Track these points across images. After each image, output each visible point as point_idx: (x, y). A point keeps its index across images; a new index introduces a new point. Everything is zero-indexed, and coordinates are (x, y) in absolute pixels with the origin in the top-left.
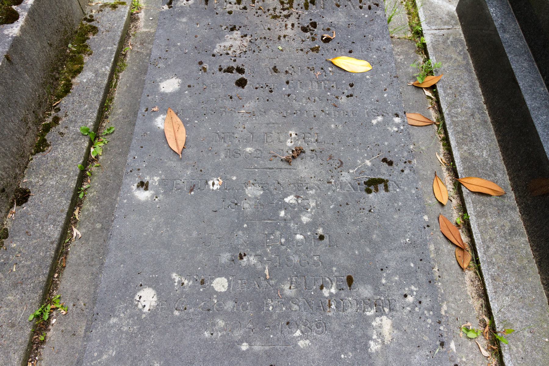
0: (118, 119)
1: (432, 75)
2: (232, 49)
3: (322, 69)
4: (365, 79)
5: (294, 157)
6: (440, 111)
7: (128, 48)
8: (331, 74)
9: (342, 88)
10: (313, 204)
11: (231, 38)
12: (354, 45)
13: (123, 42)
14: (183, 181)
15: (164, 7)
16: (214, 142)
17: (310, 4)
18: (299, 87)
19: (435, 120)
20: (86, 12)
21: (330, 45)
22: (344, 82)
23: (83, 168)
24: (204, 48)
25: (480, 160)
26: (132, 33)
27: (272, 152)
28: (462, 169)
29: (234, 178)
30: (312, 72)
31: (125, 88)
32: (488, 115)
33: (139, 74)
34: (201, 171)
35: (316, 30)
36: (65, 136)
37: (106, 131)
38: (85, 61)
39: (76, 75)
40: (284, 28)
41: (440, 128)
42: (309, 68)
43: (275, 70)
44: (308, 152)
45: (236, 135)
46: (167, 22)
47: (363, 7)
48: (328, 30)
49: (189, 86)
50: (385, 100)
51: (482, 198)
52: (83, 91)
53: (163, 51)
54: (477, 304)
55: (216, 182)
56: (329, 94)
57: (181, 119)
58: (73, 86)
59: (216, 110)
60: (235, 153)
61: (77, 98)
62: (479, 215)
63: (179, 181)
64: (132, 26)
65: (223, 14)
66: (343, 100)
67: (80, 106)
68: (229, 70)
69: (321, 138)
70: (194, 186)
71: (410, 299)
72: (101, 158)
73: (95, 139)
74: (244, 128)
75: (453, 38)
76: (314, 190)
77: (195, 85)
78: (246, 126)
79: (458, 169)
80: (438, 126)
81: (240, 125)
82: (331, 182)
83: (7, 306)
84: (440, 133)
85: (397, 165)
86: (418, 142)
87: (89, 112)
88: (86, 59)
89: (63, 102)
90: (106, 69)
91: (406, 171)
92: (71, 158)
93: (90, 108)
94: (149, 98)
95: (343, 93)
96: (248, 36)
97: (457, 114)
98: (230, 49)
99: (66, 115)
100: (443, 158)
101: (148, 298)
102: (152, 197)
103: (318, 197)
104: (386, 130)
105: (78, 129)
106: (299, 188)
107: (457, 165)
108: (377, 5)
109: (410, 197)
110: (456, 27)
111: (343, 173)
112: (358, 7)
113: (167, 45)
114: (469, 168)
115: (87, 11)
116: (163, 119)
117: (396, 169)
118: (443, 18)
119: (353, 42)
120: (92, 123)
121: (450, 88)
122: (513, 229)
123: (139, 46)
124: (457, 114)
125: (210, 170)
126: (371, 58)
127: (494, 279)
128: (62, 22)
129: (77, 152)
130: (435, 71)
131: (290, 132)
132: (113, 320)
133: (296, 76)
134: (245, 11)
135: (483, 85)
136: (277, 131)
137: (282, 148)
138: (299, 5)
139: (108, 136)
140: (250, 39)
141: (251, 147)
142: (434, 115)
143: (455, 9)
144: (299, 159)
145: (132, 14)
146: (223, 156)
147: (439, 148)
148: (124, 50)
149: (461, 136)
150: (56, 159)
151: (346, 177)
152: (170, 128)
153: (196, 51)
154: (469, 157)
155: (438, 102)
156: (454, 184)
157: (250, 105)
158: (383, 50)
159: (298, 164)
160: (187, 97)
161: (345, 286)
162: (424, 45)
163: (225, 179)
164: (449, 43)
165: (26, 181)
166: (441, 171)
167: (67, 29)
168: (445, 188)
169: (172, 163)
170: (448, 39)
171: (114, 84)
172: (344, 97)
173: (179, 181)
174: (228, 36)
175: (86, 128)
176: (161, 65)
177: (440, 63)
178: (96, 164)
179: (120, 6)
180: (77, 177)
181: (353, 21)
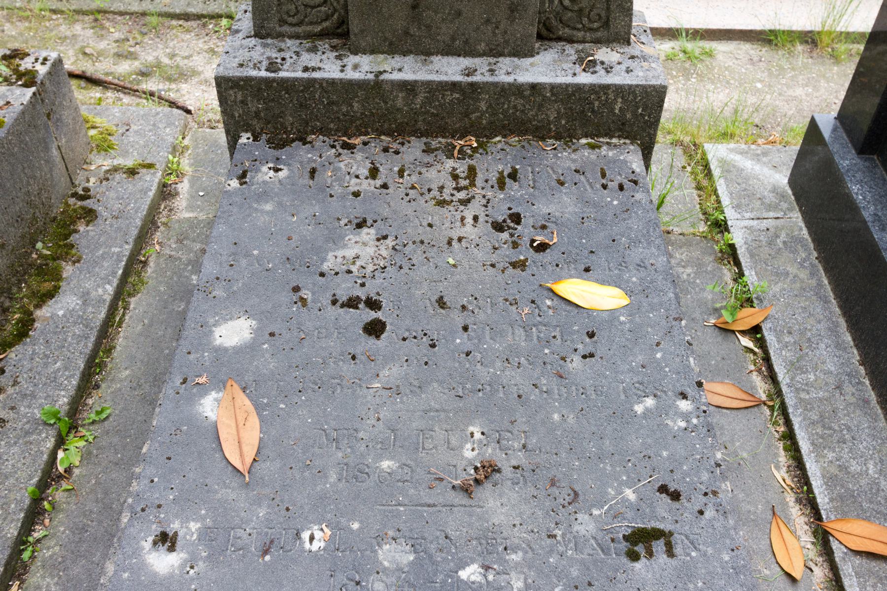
0: (120, 390)
1: (752, 306)
2: (358, 263)
3: (533, 302)
4: (617, 323)
5: (477, 482)
6: (772, 377)
7: (152, 250)
8: (551, 312)
9: (572, 341)
11: (356, 242)
12: (593, 257)
13: (149, 225)
14: (249, 535)
15: (231, 182)
16: (316, 449)
17: (507, 180)
18: (488, 338)
19: (764, 397)
20: (77, 183)
21: (546, 257)
22: (576, 328)
23: (38, 493)
24: (304, 260)
25: (863, 482)
26: (163, 220)
27: (433, 470)
28: (827, 500)
29: (356, 526)
30: (514, 308)
31: (140, 327)
32: (870, 387)
33: (170, 300)
34: (288, 509)
35: (519, 227)
36: (8, 425)
37: (93, 416)
38: (64, 276)
39: (44, 302)
40: (458, 224)
41: (775, 414)
42: (506, 300)
43: (441, 303)
44: (507, 471)
45: (361, 435)
46: (235, 210)
47: (609, 186)
48: (544, 227)
49: (272, 334)
50: (659, 364)
51: (874, 565)
52: (55, 333)
53: (225, 265)
55: (318, 535)
56: (547, 351)
57: (251, 400)
58: (36, 325)
59: (323, 383)
60: (357, 472)
61: (40, 348)
63: (240, 532)
64: (162, 207)
65: (343, 197)
66: (576, 363)
67: (46, 365)
68: (352, 303)
70: (272, 542)
72: (76, 471)
73: (69, 432)
74: (379, 419)
75: (788, 234)
76: (520, 554)
77: (284, 332)
78: (381, 416)
79: (819, 500)
80: (772, 408)
81: (372, 412)
82: (555, 536)
84: (775, 423)
85: (689, 500)
86: (732, 441)
87: (62, 376)
88: (68, 270)
89: (13, 355)
90: (105, 291)
91: (709, 514)
92: (16, 472)
93: (66, 368)
94: (191, 357)
95: (576, 350)
96: (390, 239)
97: (807, 384)
98: (354, 263)
99: (15, 383)
100: (786, 476)
102: (182, 566)
103: (530, 568)
104: (663, 426)
105: (36, 411)
107: (816, 491)
108: (635, 182)
109: (720, 570)
110: (791, 215)
111: (580, 516)
112: (598, 186)
113: (234, 254)
114: (841, 498)
115: (80, 179)
116: (216, 400)
117: (689, 507)
118: (764, 197)
119: (592, 252)
120: (66, 400)
121: (790, 333)
123: (174, 246)
124: (807, 384)
125: (307, 508)
126: (628, 281)
128: (30, 203)
129: (28, 461)
130: (757, 298)
131: (471, 429)
133: (481, 316)
134: (385, 191)
135: (854, 326)
136: (445, 426)
137: (454, 463)
138: (487, 181)
139: (96, 427)
140: (394, 243)
141: (392, 458)
142: (761, 388)
143: (786, 181)
144: (488, 485)
145: (165, 185)
146: (333, 478)
147: (776, 455)
148: (143, 252)
149: (819, 430)
151: (586, 525)
152: (230, 418)
153: (288, 266)
154: (841, 475)
155: (767, 359)
156: (815, 534)
157: (391, 373)
158: (649, 266)
159: (486, 495)
160: (267, 356)
162: (732, 247)
163: (335, 527)
164: (781, 245)
166: (785, 504)
167: (38, 214)
168: (795, 541)
169: (229, 493)
170: (778, 236)
171: (117, 319)
172: (577, 358)
173: (240, 532)
174: (352, 237)
175: (53, 410)
176: (219, 292)
177: (765, 284)
178: (65, 485)
179: (144, 171)
180: (22, 515)
181: (590, 211)
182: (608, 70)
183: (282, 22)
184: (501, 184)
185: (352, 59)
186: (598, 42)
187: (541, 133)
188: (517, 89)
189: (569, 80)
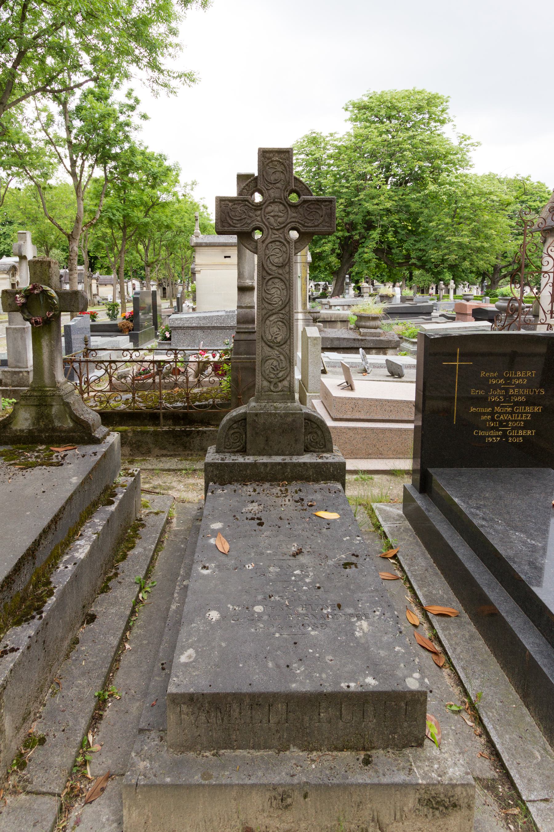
6: (403, 570)
10: (311, 574)
13: (163, 532)
43: (281, 518)
54: (456, 690)
62: (443, 629)
66: (325, 530)
68: (253, 519)
69: (313, 546)
71: (377, 613)
83: (77, 687)
88: (137, 541)
101: (214, 615)
106: (302, 567)
122: (472, 637)
127: (464, 669)
132: (193, 625)
146: (253, 554)
150: (116, 597)
155: (401, 566)
161: (337, 608)
165: (93, 610)
169: (223, 558)
182: (327, 458)
183: (225, 448)
184: (296, 492)
185: (247, 457)
186: (323, 452)
187: (308, 479)
188: (299, 464)
189: (315, 461)
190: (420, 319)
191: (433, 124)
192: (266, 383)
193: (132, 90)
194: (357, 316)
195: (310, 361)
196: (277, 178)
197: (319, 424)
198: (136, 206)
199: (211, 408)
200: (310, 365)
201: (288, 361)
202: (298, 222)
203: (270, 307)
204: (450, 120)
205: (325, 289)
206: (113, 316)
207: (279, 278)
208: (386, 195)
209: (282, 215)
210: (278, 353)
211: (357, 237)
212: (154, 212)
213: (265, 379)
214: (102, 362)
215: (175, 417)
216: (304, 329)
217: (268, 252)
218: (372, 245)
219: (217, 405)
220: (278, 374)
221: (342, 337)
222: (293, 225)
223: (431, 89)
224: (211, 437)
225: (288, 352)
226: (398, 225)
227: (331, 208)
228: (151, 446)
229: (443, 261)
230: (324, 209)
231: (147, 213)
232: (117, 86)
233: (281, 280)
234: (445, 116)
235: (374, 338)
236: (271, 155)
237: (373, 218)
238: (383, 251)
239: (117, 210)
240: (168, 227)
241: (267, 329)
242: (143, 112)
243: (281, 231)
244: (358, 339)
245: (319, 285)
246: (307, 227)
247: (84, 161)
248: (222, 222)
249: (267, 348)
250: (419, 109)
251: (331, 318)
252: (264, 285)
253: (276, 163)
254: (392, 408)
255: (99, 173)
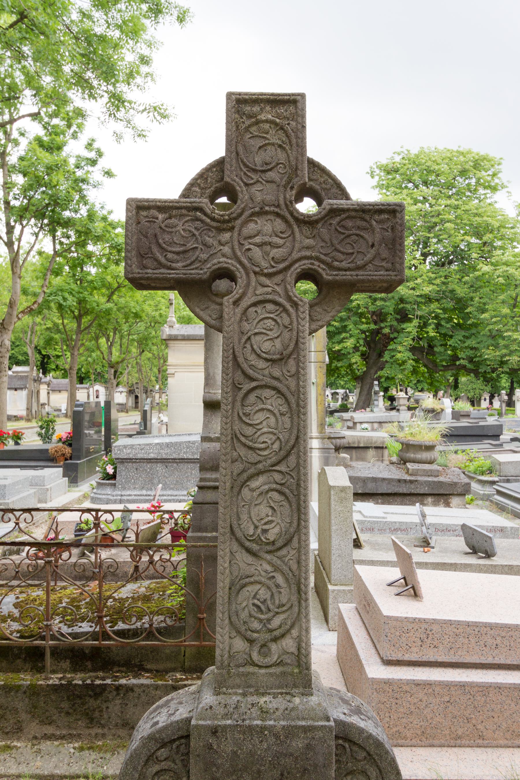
190: (486, 444)
191: (481, 191)
192: (240, 644)
193: (93, 140)
194: (402, 444)
195: (334, 528)
196: (268, 160)
197: (372, 751)
198: (95, 288)
199: (147, 639)
200: (333, 535)
201: (294, 588)
202: (318, 259)
203: (253, 457)
204: (503, 187)
205: (346, 397)
206: (46, 437)
207: (274, 388)
208: (424, 277)
209: (280, 241)
210: (269, 568)
211: (387, 331)
212: (121, 297)
213: (238, 632)
214: (12, 511)
215: (78, 656)
216: (323, 470)
217: (246, 326)
218: (408, 342)
219: (159, 630)
220: (269, 620)
221: (380, 476)
222: (305, 264)
223: (479, 148)
224: (144, 698)
225: (294, 567)
226: (442, 316)
227: (393, 228)
228: (24, 716)
229: (502, 363)
230: (378, 233)
231: (110, 298)
232: (74, 136)
233: (279, 392)
234: (497, 181)
235: (430, 479)
236: (256, 109)
237: (408, 306)
238: (423, 351)
239: (71, 293)
240: (137, 315)
241: (245, 510)
242: (107, 167)
243: (278, 279)
244: (405, 481)
245: (337, 394)
246: (339, 269)
247: (23, 227)
248: (141, 256)
249: (242, 557)
250: (463, 173)
251: (359, 442)
252: (238, 404)
253: (267, 126)
254: (499, 640)
255: (47, 245)
